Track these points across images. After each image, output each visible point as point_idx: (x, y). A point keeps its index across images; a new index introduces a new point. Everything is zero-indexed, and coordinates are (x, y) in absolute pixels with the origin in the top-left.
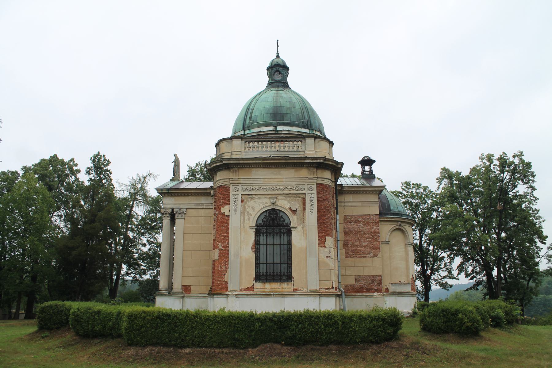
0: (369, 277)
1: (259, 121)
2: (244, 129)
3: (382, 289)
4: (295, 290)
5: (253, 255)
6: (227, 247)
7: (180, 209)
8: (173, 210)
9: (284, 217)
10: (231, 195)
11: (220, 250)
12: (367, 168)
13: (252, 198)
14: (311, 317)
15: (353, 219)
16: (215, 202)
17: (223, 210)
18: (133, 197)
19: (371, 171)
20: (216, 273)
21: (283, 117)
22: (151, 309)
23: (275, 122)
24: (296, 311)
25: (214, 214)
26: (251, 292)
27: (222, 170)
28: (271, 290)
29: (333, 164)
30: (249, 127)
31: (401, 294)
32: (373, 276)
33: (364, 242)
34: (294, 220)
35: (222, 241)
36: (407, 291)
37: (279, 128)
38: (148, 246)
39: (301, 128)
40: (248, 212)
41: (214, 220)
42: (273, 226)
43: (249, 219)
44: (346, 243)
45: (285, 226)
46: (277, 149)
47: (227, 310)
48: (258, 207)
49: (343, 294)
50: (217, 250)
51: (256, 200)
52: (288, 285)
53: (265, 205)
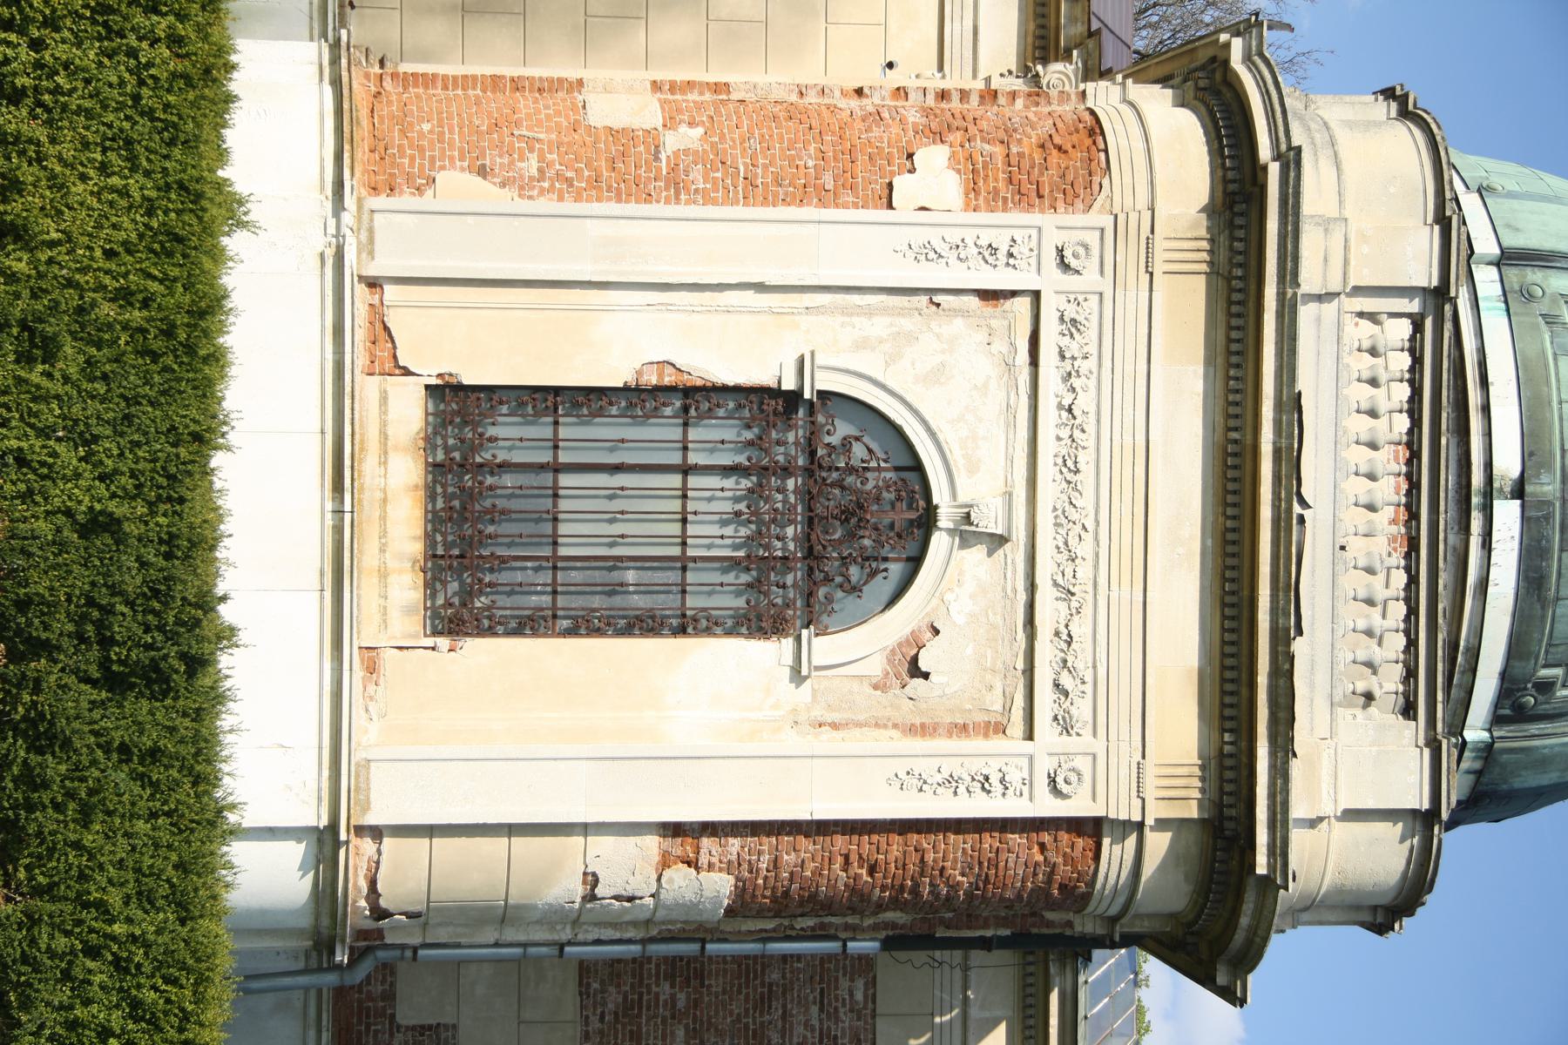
2: (1508, 258)
5: (614, 376)
6: (676, 185)
9: (881, 587)
10: (1035, 218)
11: (653, 143)
13: (1009, 366)
14: (197, 664)
15: (846, 1020)
16: (990, 95)
20: (495, 103)
23: (1547, 486)
24: (228, 739)
25: (901, 92)
26: (362, 361)
28: (370, 497)
29: (1239, 938)
30: (1527, 295)
34: (857, 646)
37: (1507, 514)
39: (1504, 675)
40: (912, 338)
41: (859, 92)
42: (827, 508)
43: (862, 345)
46: (1357, 547)
47: (234, 242)
48: (951, 401)
49: (331, 979)
50: (644, 113)
51: (998, 395)
52: (409, 611)
53: (956, 457)
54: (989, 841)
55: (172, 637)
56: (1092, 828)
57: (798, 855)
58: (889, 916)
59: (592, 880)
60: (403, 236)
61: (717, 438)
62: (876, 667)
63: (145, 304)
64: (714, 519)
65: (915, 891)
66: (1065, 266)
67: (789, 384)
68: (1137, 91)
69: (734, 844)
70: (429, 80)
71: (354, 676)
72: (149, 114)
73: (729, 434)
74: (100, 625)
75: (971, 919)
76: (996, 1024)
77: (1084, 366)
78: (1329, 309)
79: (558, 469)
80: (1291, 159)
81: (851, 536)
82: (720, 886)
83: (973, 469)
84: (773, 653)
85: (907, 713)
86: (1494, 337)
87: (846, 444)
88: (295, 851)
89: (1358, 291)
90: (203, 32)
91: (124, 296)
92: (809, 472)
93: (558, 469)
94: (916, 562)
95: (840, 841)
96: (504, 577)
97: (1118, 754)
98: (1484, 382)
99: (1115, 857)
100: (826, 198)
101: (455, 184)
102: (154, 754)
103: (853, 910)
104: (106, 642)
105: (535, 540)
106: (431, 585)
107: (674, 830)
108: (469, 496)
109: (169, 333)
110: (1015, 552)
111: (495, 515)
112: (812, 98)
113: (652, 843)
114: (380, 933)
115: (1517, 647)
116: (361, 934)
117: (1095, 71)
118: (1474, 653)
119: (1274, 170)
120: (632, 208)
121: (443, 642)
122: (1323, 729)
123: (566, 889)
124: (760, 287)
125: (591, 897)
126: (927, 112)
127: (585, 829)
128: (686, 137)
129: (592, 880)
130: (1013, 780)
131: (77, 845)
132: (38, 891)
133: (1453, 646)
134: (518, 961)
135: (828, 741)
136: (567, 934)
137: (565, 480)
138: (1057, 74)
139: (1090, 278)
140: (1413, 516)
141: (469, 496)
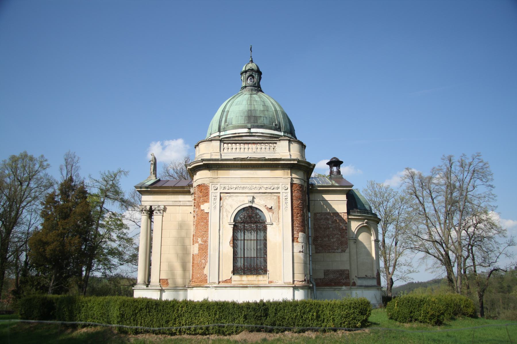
0: (338, 271)
1: (234, 123)
2: (219, 131)
3: (349, 283)
4: (270, 282)
5: (231, 250)
6: (206, 242)
7: (159, 206)
8: (151, 207)
9: (260, 213)
10: (210, 193)
12: (335, 169)
13: (230, 196)
14: (264, 304)
15: (322, 217)
16: (195, 200)
17: (202, 207)
18: (105, 193)
19: (339, 172)
21: (257, 120)
22: (132, 298)
23: (249, 125)
25: (194, 211)
26: (230, 284)
27: (202, 170)
28: (248, 283)
29: (306, 165)
31: (367, 287)
32: (341, 270)
33: (333, 238)
34: (268, 216)
35: (202, 236)
36: (373, 285)
37: (253, 130)
38: (118, 242)
40: (226, 210)
42: (249, 221)
43: (227, 216)
44: (315, 239)
45: (261, 223)
46: (254, 150)
47: (210, 300)
48: (235, 204)
50: (197, 245)
51: (234, 198)
52: (263, 277)
53: (242, 203)
54: (294, 198)
55: (260, 308)
56: (292, 184)
57: (296, 224)
58: (305, 211)
59: (300, 252)
60: (213, 278)
61: (240, 236)
62: (271, 214)
63: (216, 311)
64: (251, 236)
65: (301, 208)
66: (217, 189)
67: (233, 226)
68: (194, 180)
69: (295, 232)
70: (193, 275)
71: (272, 285)
72: (191, 311)
73: (239, 234)
74: (259, 317)
75: (305, 200)
76: (323, 197)
77: (230, 186)
78: (222, 155)
79: (244, 257)
80: (203, 160)
81: (253, 217)
82: (301, 234)
83: (244, 201)
84: (269, 228)
85: (277, 209)
86: (230, 132)
87: (240, 218)
88: (296, 292)
89: (220, 151)
90: (181, 303)
91: (215, 314)
92: (244, 223)
93: (244, 257)
94: (256, 209)
95: (294, 218)
96: (259, 264)
97: (282, 181)
98: (235, 134)
99: (296, 181)
100: (207, 221)
101: (206, 271)
102: (276, 310)
103: (304, 216)
104: (261, 316)
105: (254, 260)
106: (260, 274)
107: (293, 241)
108: (248, 269)
109: (220, 308)
110: (255, 195)
111: (250, 266)
112: (195, 223)
113: (295, 244)
114: (308, 280)
115: (271, 129)
116: (308, 283)
117: (192, 186)
118: (271, 134)
119: (204, 162)
120: (209, 247)
121: (268, 272)
122: (278, 154)
123: (301, 255)
124: (219, 230)
125: (302, 252)
126: (197, 208)
127: (293, 253)
128: (199, 240)
129: (300, 252)
130: (286, 196)
131: (288, 319)
132: (294, 324)
133: (270, 137)
134: (312, 261)
135: (281, 220)
136: (308, 255)
137: (246, 256)
138: (192, 191)
139: (218, 186)
140: (258, 143)
141: (248, 269)
